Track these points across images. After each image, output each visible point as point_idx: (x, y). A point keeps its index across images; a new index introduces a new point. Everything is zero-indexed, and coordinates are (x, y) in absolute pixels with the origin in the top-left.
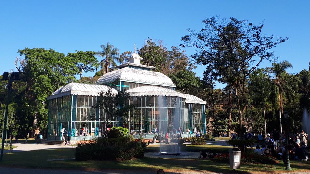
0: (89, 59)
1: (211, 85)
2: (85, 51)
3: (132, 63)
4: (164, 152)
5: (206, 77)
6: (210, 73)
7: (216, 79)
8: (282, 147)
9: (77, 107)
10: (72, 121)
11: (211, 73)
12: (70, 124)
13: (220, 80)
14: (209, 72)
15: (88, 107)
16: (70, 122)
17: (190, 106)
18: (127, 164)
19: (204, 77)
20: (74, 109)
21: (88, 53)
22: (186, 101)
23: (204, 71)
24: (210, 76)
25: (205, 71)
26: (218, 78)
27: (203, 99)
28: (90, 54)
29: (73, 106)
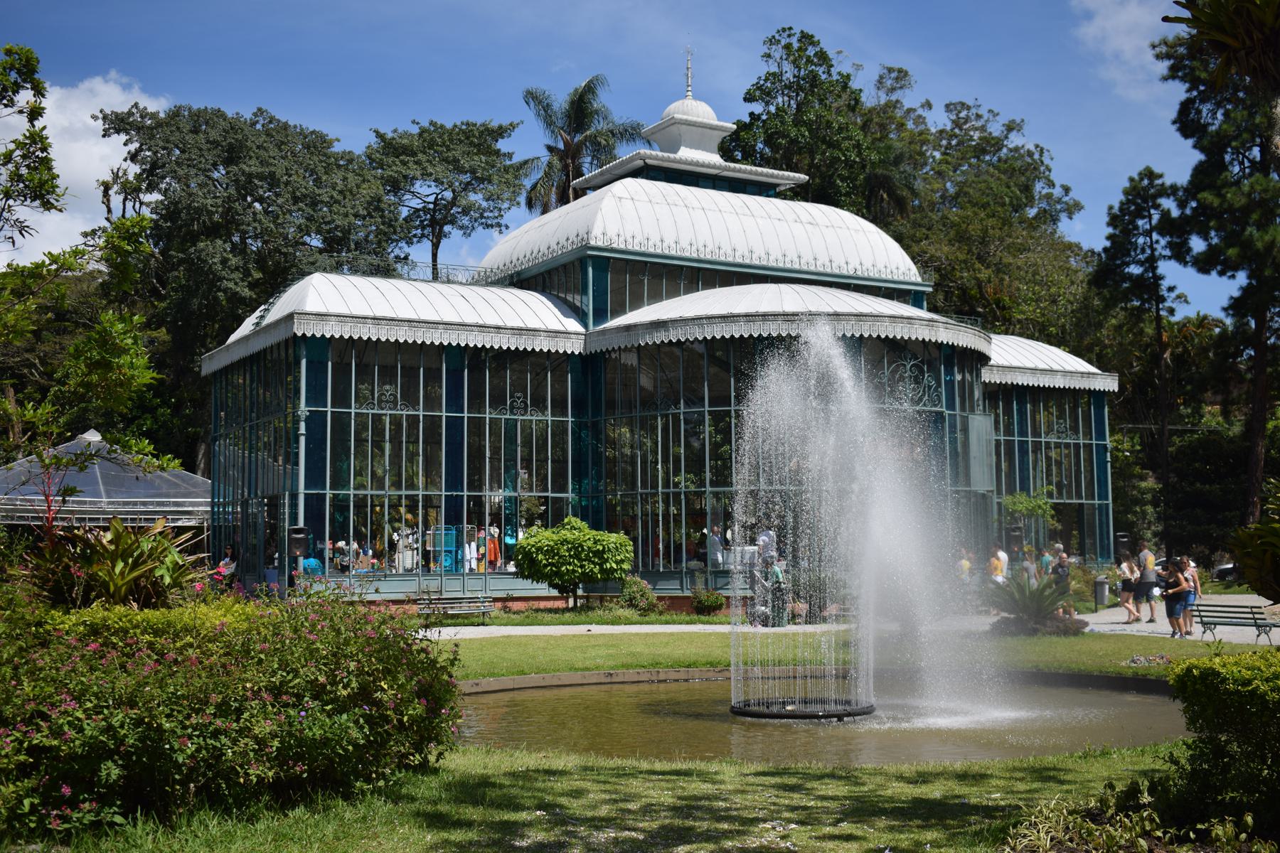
0: (479, 160)
1: (1150, 287)
2: (449, 120)
3: (672, 156)
4: (661, 546)
5: (1120, 245)
6: (1143, 217)
7: (1180, 253)
8: (587, 165)
9: (329, 409)
10: (306, 488)
11: (1150, 217)
12: (294, 505)
13: (1204, 264)
14: (1139, 213)
15: (395, 408)
16: (294, 497)
17: (1013, 399)
18: (714, 782)
19: (1108, 244)
20: (316, 421)
21: (584, 194)
22: (987, 376)
23: (1111, 208)
24: (1148, 233)
25: (1117, 206)
26: (1197, 245)
27: (1103, 364)
28: (482, 139)
29: (308, 404)
